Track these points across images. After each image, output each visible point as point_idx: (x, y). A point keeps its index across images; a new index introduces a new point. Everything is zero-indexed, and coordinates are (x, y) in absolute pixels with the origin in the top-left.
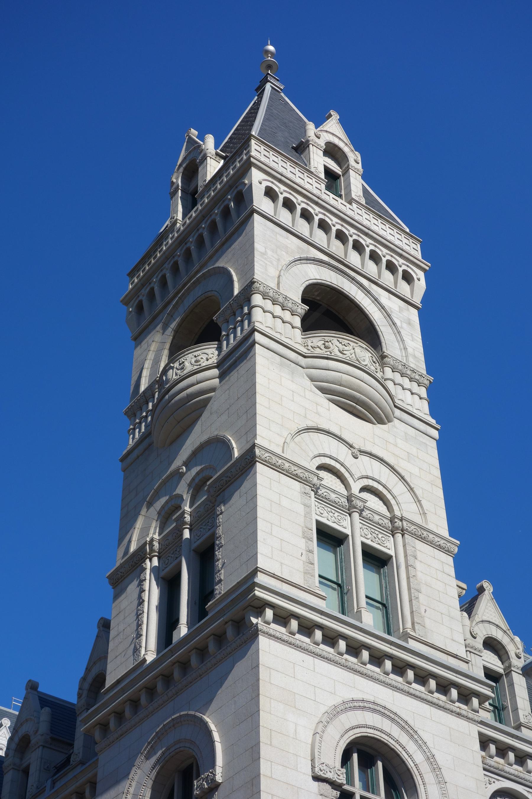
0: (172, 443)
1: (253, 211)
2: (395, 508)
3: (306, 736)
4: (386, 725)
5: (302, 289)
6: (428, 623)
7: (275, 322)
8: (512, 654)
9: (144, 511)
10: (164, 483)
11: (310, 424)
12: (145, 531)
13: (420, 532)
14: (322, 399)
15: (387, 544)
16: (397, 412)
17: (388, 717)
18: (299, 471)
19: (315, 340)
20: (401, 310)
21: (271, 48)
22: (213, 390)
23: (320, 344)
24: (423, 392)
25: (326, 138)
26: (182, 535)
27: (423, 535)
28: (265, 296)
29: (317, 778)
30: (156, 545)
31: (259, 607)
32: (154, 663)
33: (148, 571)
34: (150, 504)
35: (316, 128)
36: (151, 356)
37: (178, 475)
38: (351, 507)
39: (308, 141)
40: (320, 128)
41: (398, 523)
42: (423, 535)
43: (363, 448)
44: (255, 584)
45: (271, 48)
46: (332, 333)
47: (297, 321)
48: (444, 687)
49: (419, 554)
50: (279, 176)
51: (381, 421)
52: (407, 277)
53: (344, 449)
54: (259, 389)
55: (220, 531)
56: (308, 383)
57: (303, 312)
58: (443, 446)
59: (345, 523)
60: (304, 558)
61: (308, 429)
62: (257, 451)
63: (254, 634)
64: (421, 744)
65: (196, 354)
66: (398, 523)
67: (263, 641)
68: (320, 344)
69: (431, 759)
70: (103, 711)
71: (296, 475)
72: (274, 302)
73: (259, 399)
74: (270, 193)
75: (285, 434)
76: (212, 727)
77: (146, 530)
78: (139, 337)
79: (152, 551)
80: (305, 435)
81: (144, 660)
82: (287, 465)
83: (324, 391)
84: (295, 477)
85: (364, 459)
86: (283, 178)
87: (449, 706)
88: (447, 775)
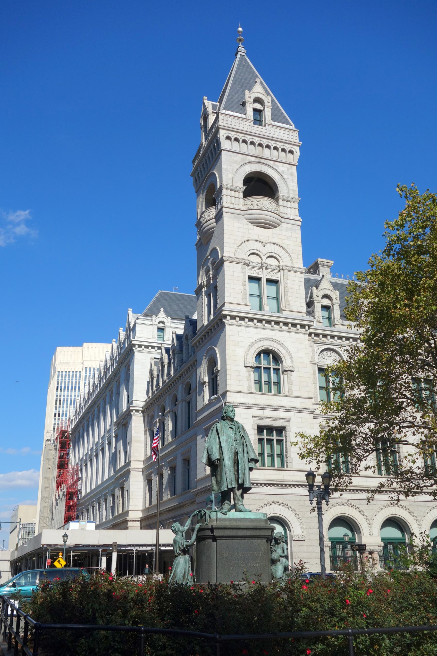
0: (207, 244)
1: (222, 150)
2: (281, 261)
3: (242, 354)
4: (272, 344)
5: (243, 179)
6: (291, 303)
7: (232, 198)
8: (334, 299)
9: (201, 269)
10: (204, 262)
11: (246, 239)
12: (202, 279)
13: (289, 268)
14: (251, 226)
15: (277, 276)
16: (283, 220)
17: (273, 341)
18: (240, 261)
19: (248, 201)
20: (288, 169)
21: (240, 29)
22: (214, 227)
23: (249, 203)
24: (296, 206)
25: (254, 96)
26: (210, 281)
27: (291, 270)
28: (227, 189)
29: (246, 367)
30: (205, 283)
31: (225, 316)
32: (207, 325)
33: (204, 292)
34: (203, 267)
35: (249, 92)
36: (200, 207)
37: (207, 259)
38: (262, 266)
39: (246, 101)
40: (251, 92)
41: (281, 268)
42: (291, 270)
43: (267, 242)
44: (222, 310)
45: (240, 29)
46: (254, 197)
47: (241, 195)
48: (294, 325)
49: (289, 278)
50: (231, 129)
51: (275, 227)
52: (291, 152)
53: (260, 244)
54: (225, 231)
55: (217, 285)
56: (245, 221)
57: (243, 190)
58: (303, 229)
59: (260, 273)
60: (243, 293)
61: (245, 242)
62: (224, 258)
63: (224, 325)
64: (285, 347)
65: (208, 212)
66: (281, 268)
67: (227, 327)
68: (249, 203)
69: (288, 351)
70: (197, 338)
71: (240, 262)
72: (231, 190)
73: (225, 236)
74: (228, 138)
75: (236, 246)
76: (217, 352)
77: (203, 279)
78: (198, 196)
79: (204, 285)
80: (244, 244)
81: (204, 325)
82: (236, 259)
83: (251, 223)
84: (239, 263)
85: (268, 245)
86: (233, 129)
87: (298, 331)
88: (293, 355)
